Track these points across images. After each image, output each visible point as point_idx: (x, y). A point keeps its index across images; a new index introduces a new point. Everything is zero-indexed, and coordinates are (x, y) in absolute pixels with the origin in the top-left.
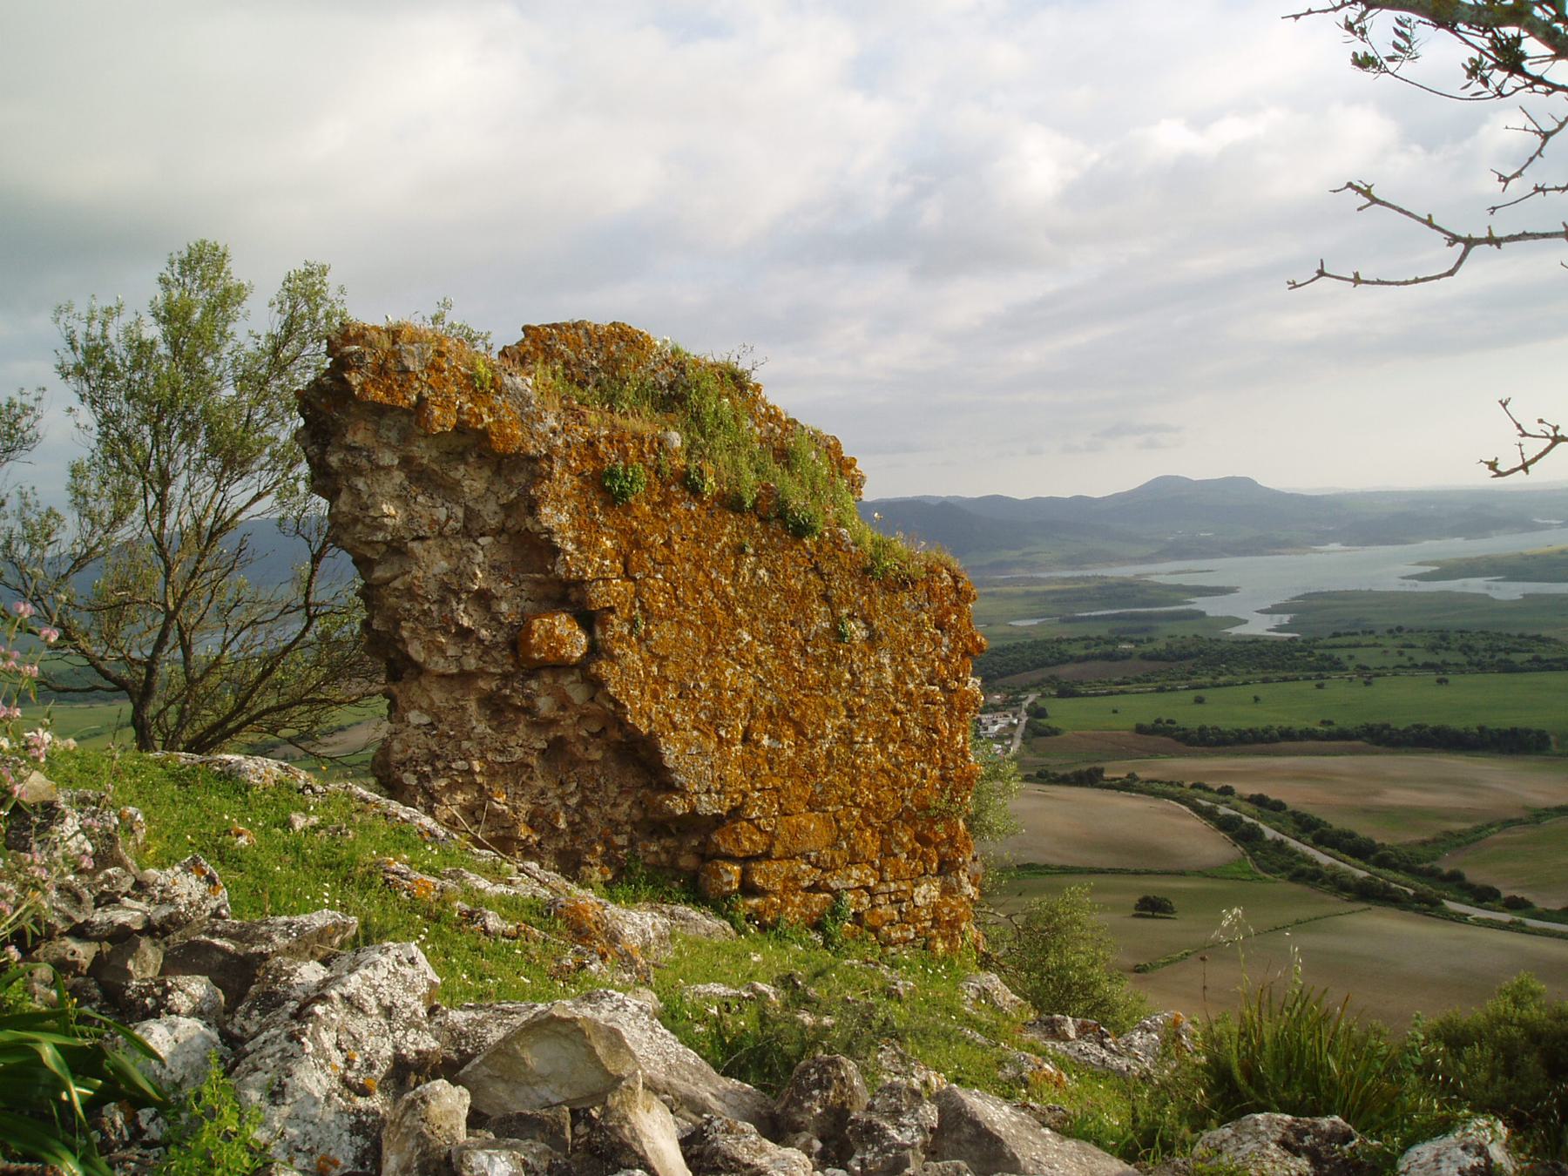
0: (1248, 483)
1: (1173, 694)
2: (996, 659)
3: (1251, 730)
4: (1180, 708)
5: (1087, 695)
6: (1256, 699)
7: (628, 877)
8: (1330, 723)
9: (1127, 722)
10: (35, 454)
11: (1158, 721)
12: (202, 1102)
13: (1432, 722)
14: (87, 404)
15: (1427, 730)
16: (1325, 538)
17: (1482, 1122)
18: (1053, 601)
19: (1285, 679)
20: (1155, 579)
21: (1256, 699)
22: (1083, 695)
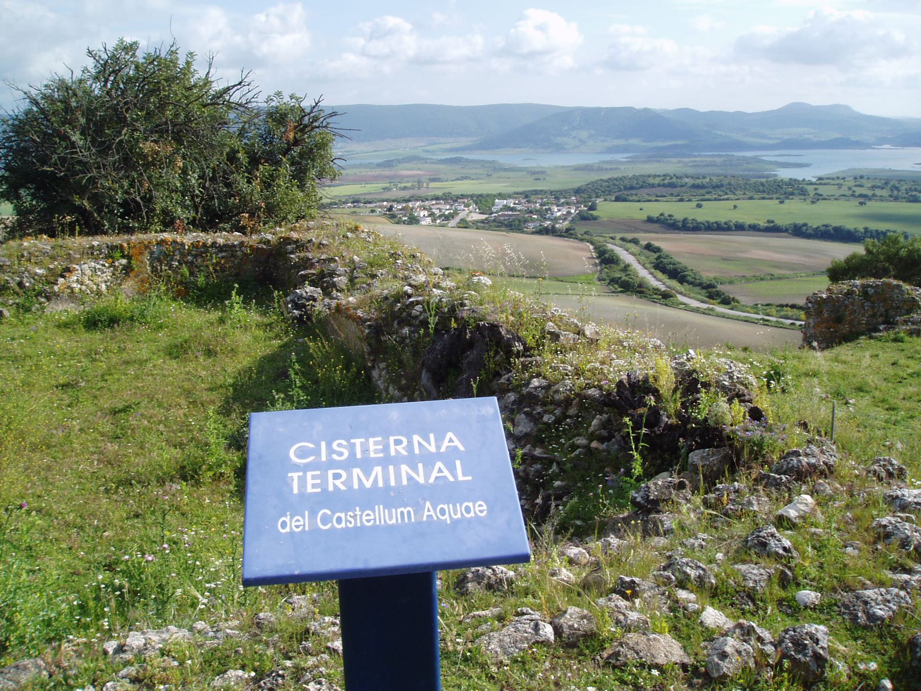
0: (847, 108)
1: (689, 203)
2: (604, 184)
3: (716, 223)
4: (679, 210)
5: (633, 201)
6: (735, 207)
7: (37, 220)
8: (772, 222)
9: (643, 216)
10: (649, 215)
11: (662, 214)
12: (576, 594)
13: (836, 223)
14: (786, 201)
15: (830, 228)
16: (881, 141)
17: (764, 406)
18: (692, 166)
19: (763, 198)
20: (763, 158)
21: (735, 207)
22: (631, 201)
